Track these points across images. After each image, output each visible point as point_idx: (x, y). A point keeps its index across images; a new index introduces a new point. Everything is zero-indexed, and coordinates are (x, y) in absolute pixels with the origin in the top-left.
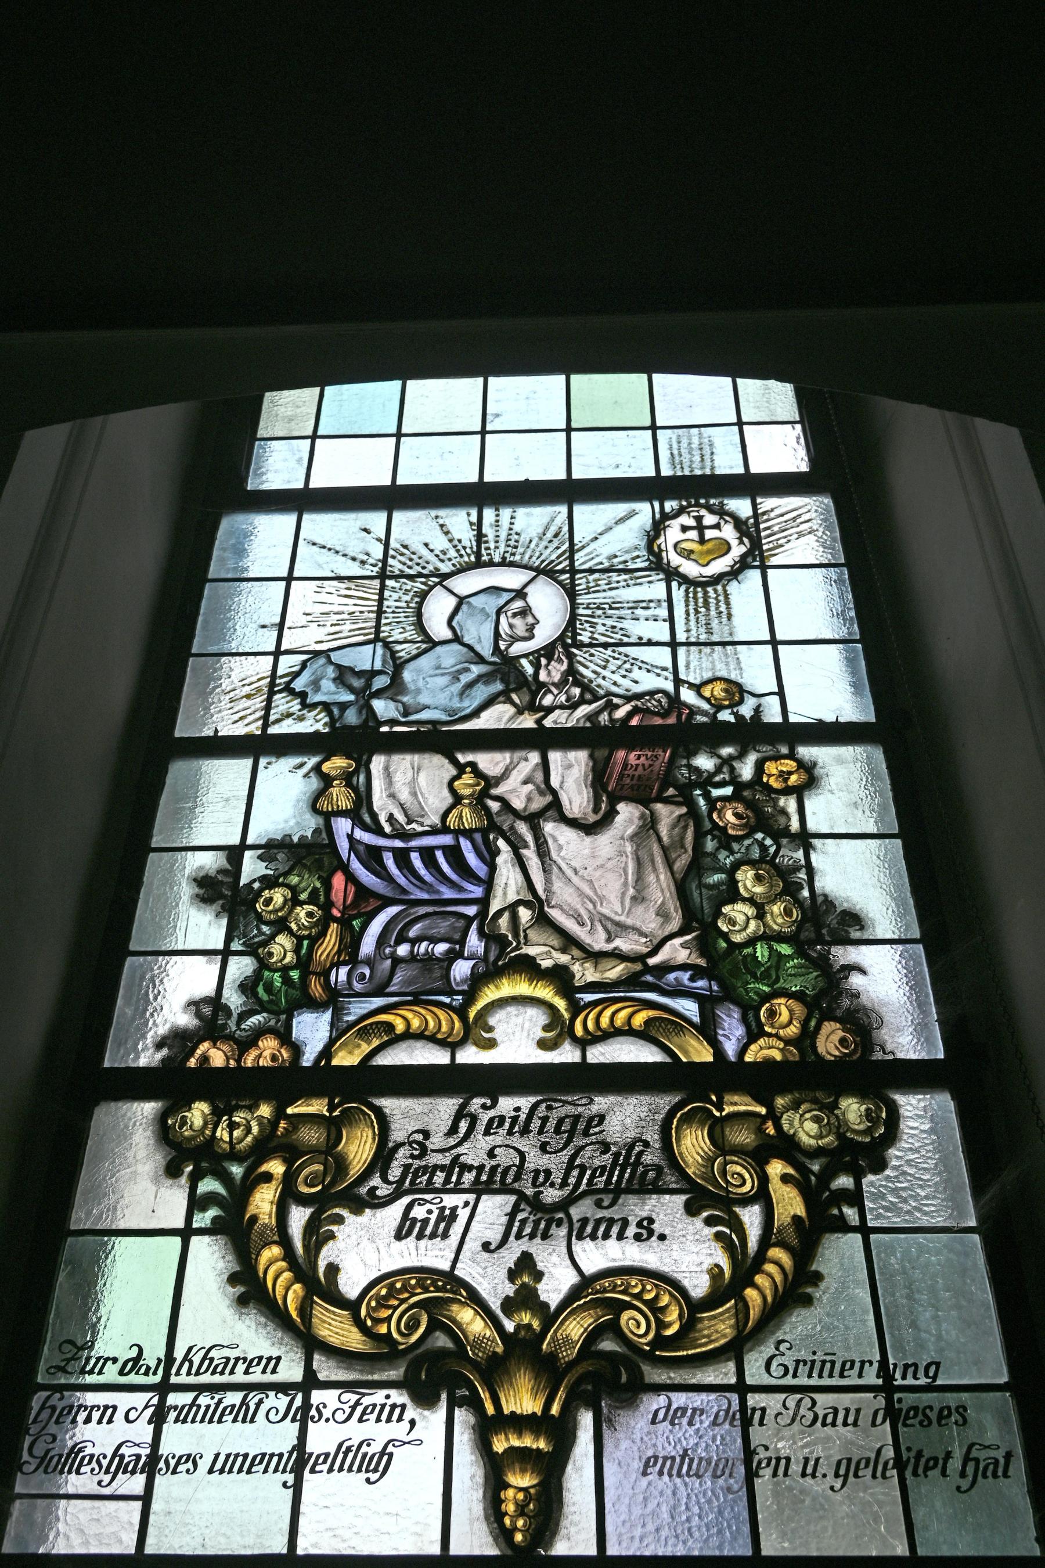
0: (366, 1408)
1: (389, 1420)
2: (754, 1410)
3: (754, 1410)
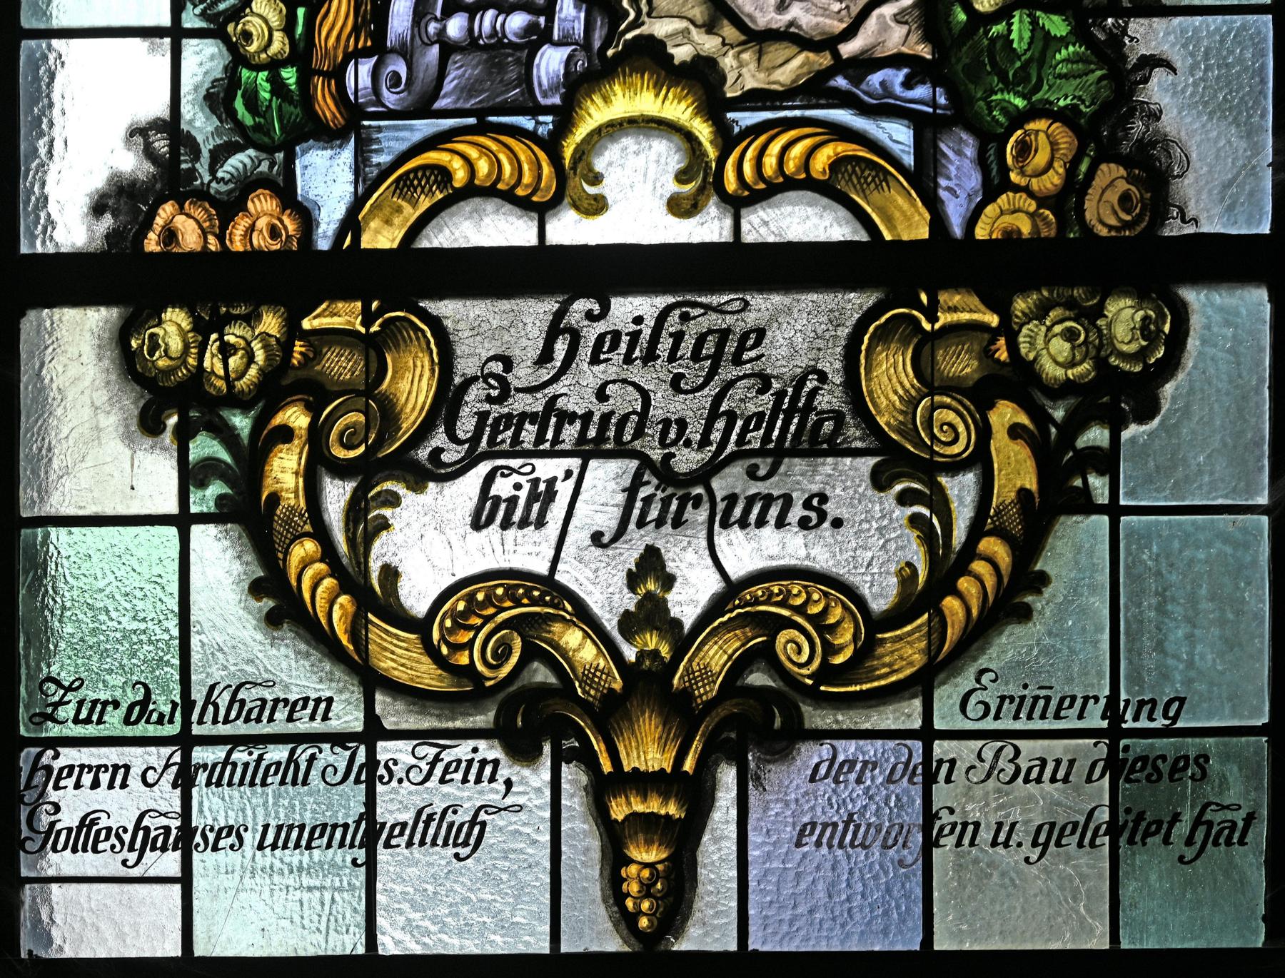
0: (449, 764)
1: (478, 780)
2: (940, 762)
3: (940, 762)
